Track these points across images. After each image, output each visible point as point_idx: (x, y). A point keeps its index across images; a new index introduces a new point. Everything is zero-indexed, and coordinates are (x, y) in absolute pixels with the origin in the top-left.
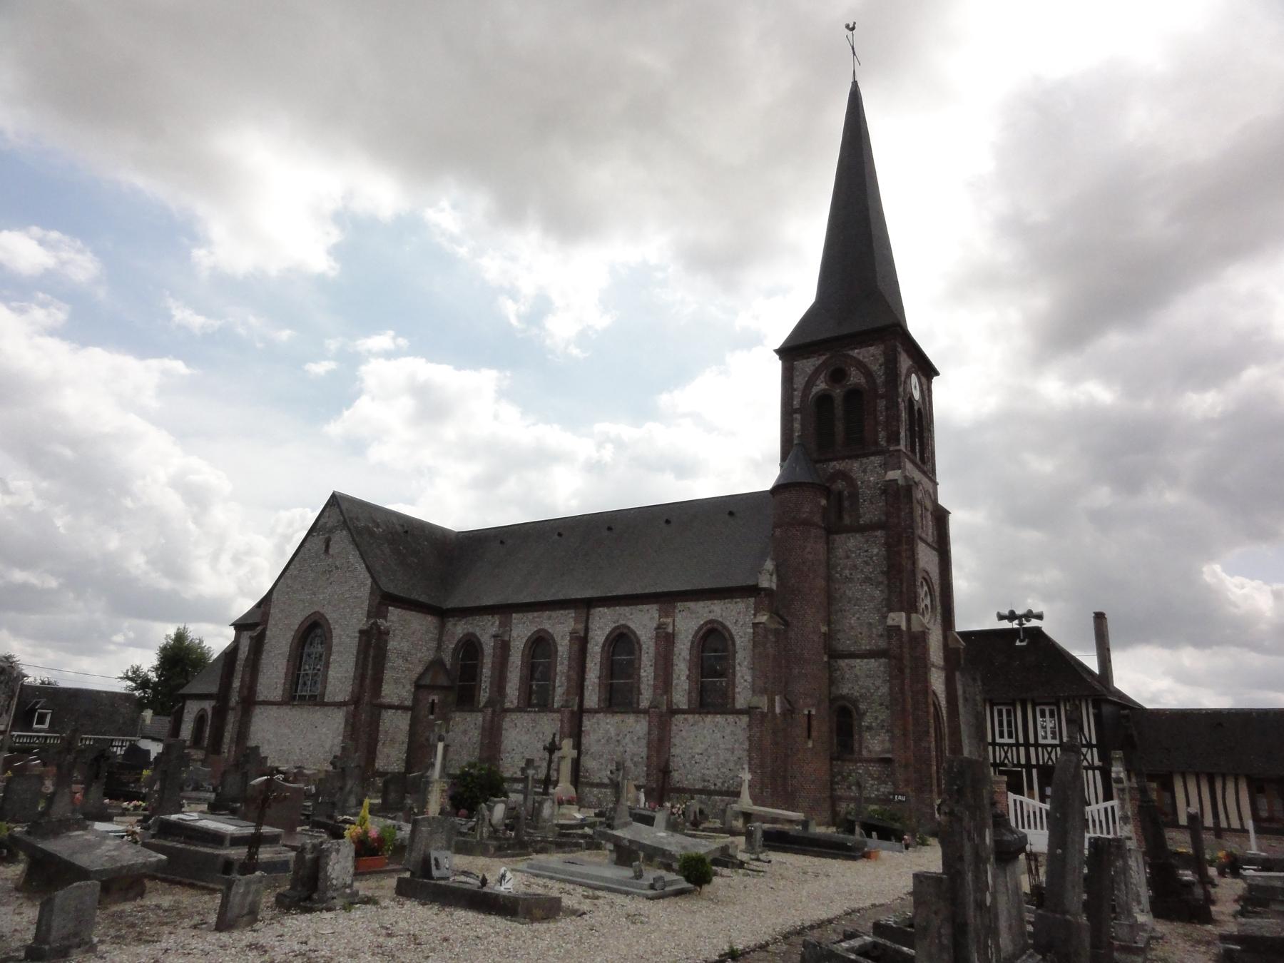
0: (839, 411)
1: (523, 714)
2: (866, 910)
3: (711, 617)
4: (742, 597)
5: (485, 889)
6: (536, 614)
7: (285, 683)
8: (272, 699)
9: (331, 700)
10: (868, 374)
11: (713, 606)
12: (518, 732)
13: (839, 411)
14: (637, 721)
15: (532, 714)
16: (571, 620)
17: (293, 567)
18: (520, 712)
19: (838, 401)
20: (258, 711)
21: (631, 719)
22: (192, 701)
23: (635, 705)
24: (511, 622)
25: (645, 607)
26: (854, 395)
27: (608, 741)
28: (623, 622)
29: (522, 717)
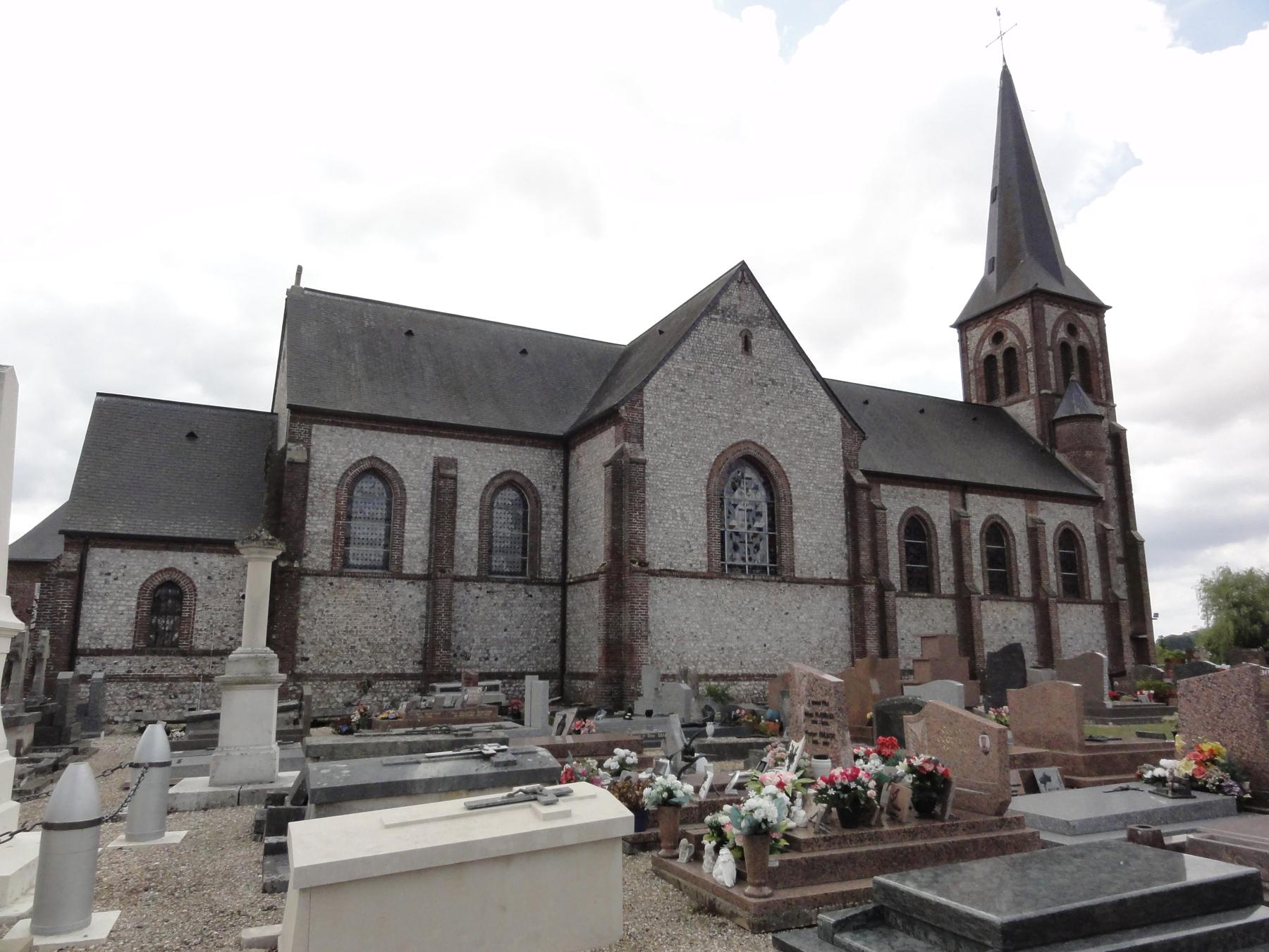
0: (1000, 364)
1: (908, 599)
2: (249, 538)
3: (1066, 518)
4: (1085, 504)
5: (1021, 783)
6: (907, 489)
7: (791, 510)
8: (684, 567)
9: (806, 576)
10: (1019, 335)
11: (1065, 509)
12: (905, 619)
13: (1000, 364)
14: (1019, 609)
15: (919, 600)
16: (946, 502)
17: (359, 495)
18: (904, 596)
19: (1000, 358)
20: (570, 588)
21: (1014, 606)
22: (1032, 609)
23: (1016, 594)
24: (879, 492)
25: (1013, 500)
26: (1010, 352)
27: (996, 628)
28: (996, 512)
29: (907, 603)
